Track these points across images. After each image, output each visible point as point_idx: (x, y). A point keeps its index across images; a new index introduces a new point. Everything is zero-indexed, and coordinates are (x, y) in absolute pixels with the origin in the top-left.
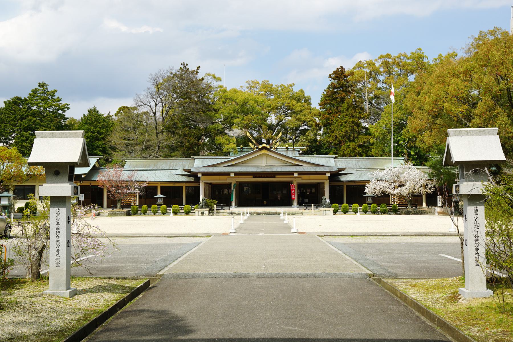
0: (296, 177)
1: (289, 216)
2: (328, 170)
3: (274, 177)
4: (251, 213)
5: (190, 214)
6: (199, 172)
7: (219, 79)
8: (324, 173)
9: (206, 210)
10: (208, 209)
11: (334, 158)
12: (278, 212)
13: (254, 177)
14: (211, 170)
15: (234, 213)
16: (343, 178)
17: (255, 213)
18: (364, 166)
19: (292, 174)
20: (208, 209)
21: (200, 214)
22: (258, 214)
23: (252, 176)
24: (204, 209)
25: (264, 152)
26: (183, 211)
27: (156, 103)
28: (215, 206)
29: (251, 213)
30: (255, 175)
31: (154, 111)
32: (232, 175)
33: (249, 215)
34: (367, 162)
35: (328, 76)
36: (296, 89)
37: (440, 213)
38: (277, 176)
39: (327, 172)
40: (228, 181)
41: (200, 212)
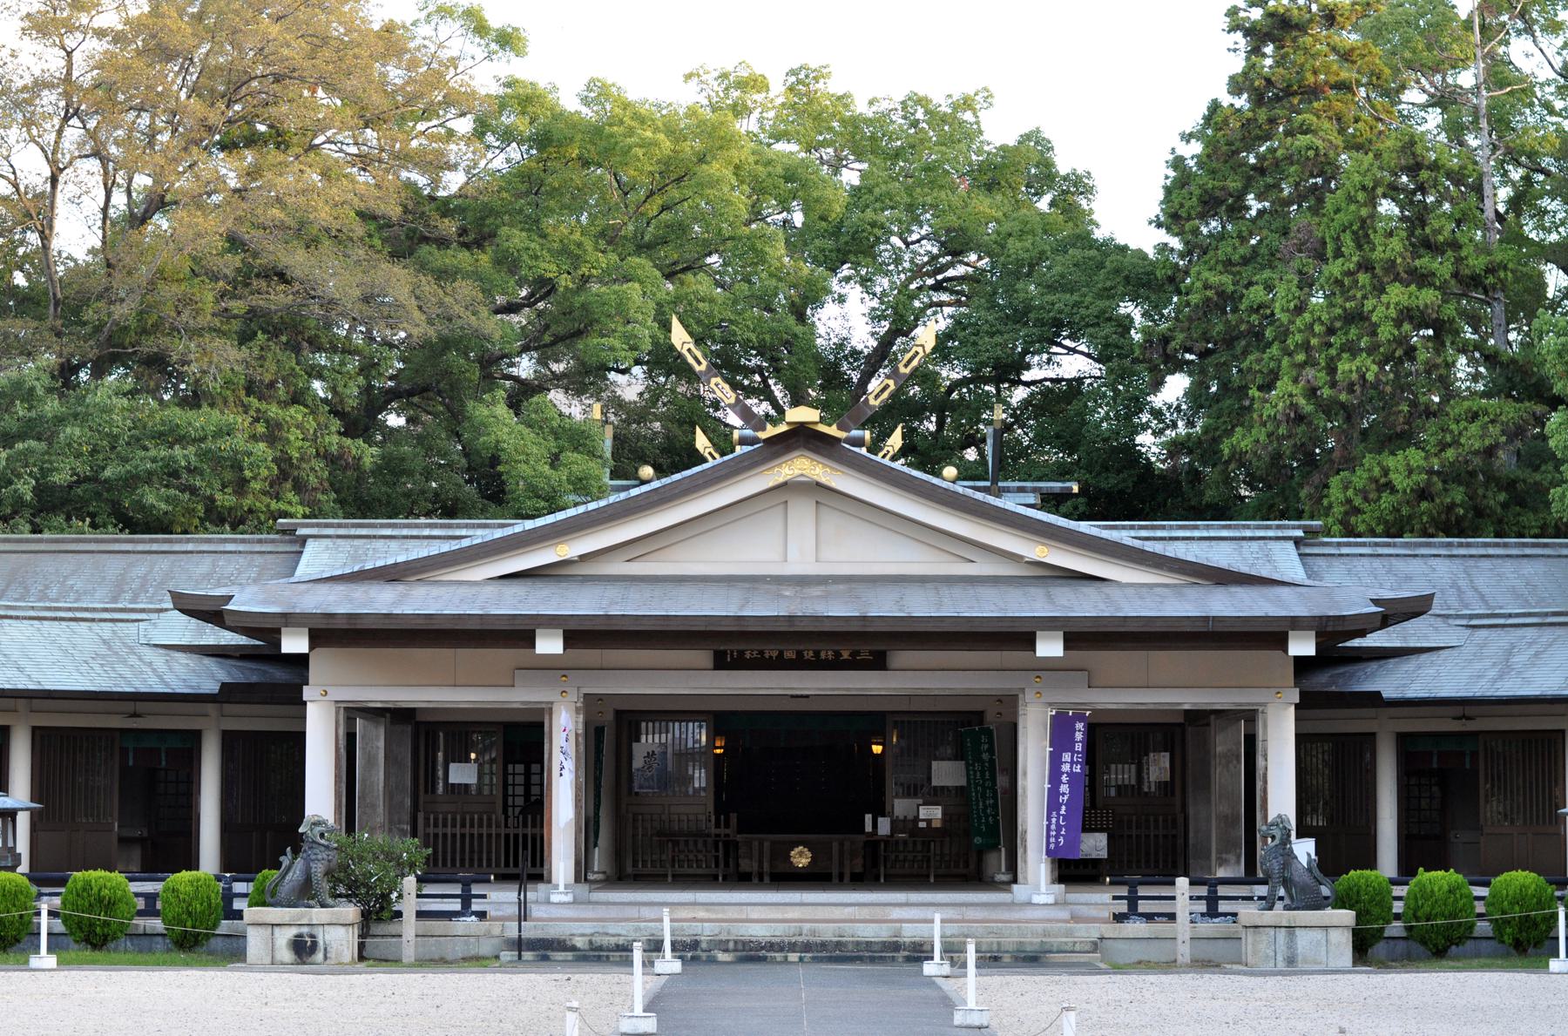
0: (1049, 665)
1: (996, 980)
2: (1300, 611)
3: (878, 662)
4: (688, 949)
5: (215, 943)
6: (291, 619)
7: (507, 40)
8: (1271, 635)
9: (336, 924)
10: (350, 912)
11: (1298, 542)
12: (910, 933)
13: (722, 662)
14: (383, 601)
15: (560, 945)
16: (1391, 683)
17: (723, 946)
18: (1516, 594)
19: (1019, 636)
20: (350, 912)
21: (286, 955)
22: (752, 954)
23: (704, 657)
24: (318, 914)
25: (800, 466)
26: (157, 924)
27: (52, 162)
28: (410, 882)
29: (688, 949)
30: (734, 645)
31: (12, 177)
32: (549, 645)
33: (669, 964)
34: (1528, 568)
35: (1225, 22)
36: (999, 130)
37: (1111, 883)
38: (900, 657)
39: (1296, 623)
40: (517, 696)
41: (284, 936)
